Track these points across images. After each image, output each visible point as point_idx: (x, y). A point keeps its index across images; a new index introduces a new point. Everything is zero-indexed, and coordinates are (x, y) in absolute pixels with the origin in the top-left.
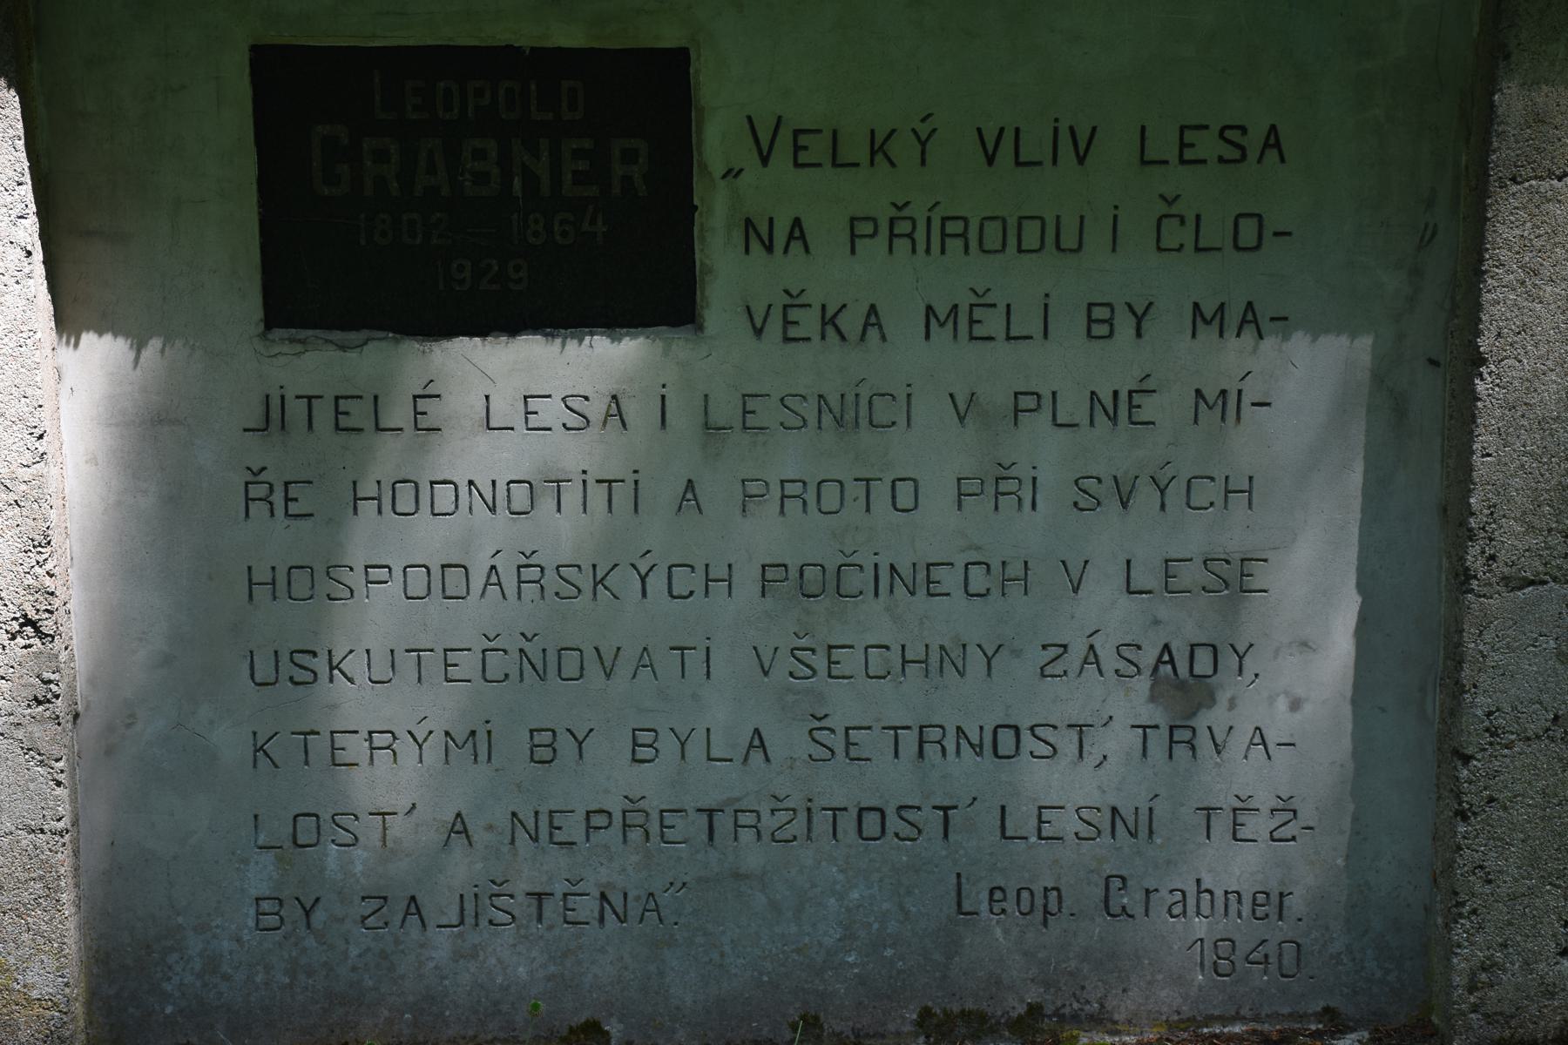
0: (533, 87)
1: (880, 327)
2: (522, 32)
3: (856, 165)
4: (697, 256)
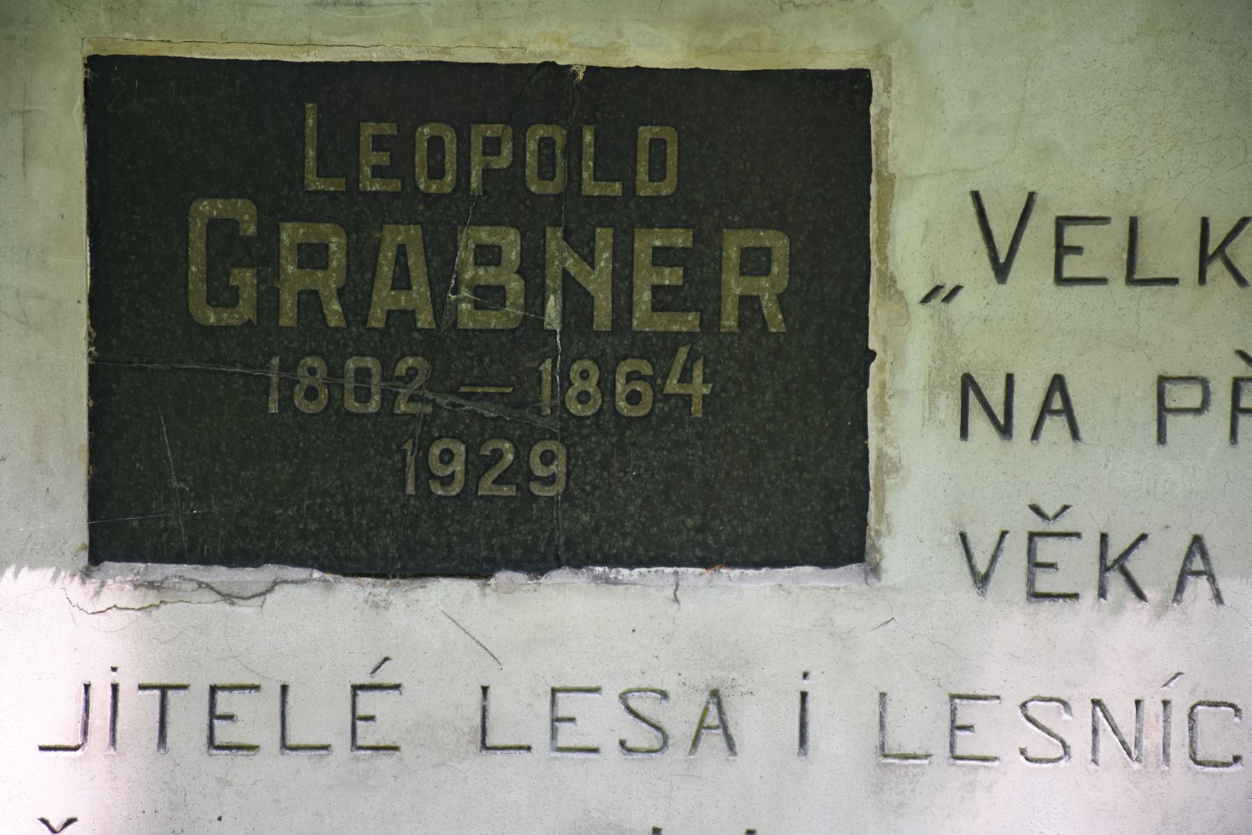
0: (588, 137)
1: (1212, 578)
2: (577, 43)
3: (1173, 281)
4: (873, 442)
